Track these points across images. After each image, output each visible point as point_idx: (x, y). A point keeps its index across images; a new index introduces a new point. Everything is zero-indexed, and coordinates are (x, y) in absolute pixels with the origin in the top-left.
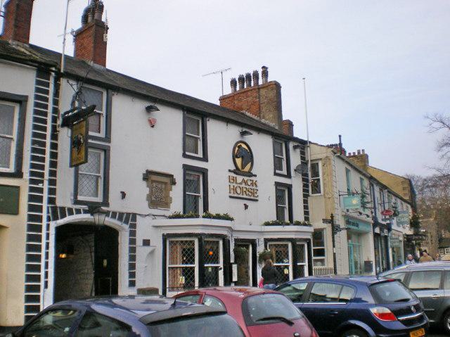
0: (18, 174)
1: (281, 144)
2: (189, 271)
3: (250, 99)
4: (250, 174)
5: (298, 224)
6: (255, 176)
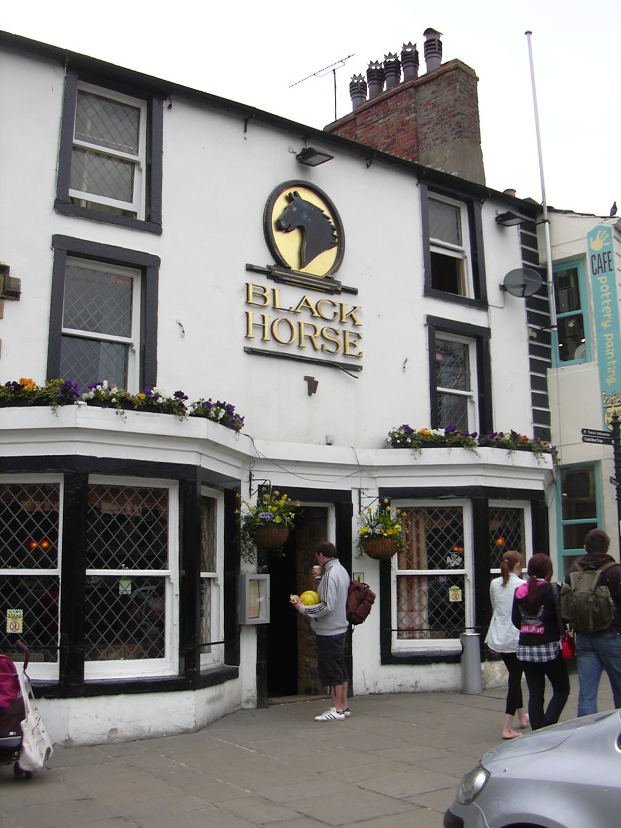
1: (458, 210)
2: (103, 591)
3: (393, 118)
5: (516, 443)
6: (354, 292)
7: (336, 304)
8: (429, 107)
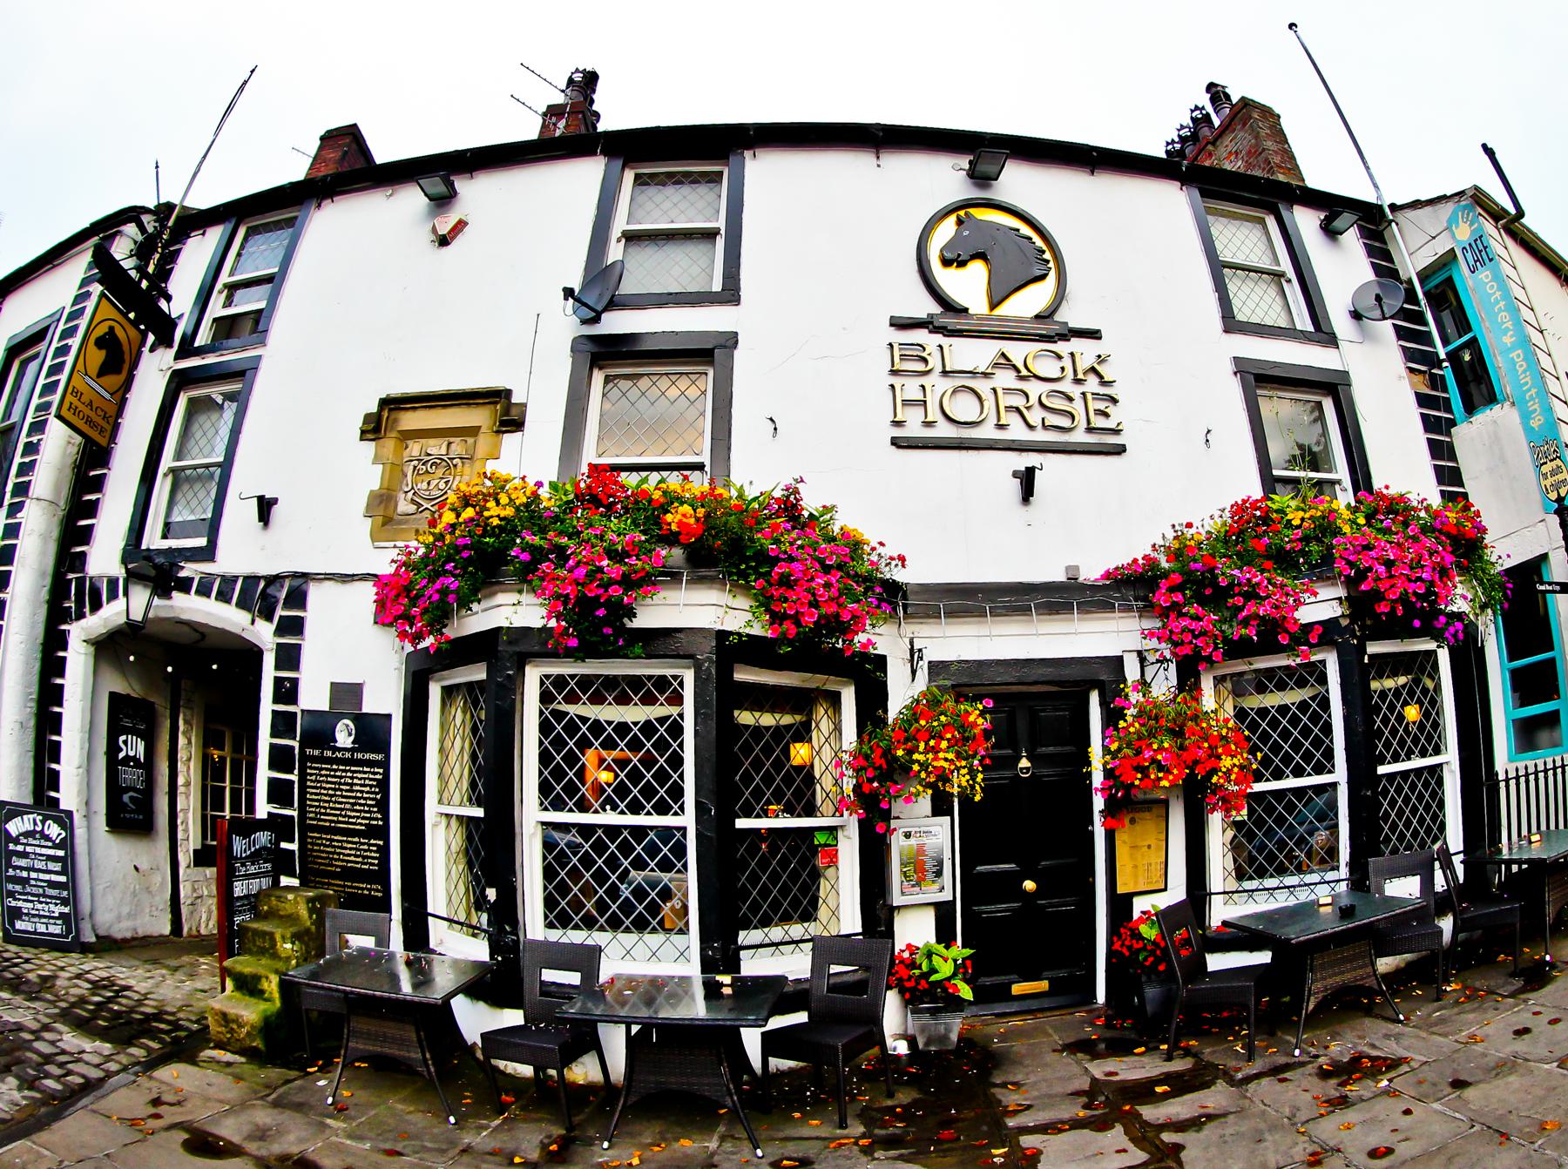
1: (1262, 222)
6: (1094, 335)
7: (1062, 354)
8: (1233, 158)
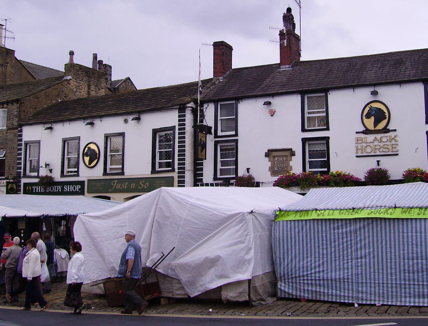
0: (173, 170)
4: (386, 130)
6: (395, 130)
